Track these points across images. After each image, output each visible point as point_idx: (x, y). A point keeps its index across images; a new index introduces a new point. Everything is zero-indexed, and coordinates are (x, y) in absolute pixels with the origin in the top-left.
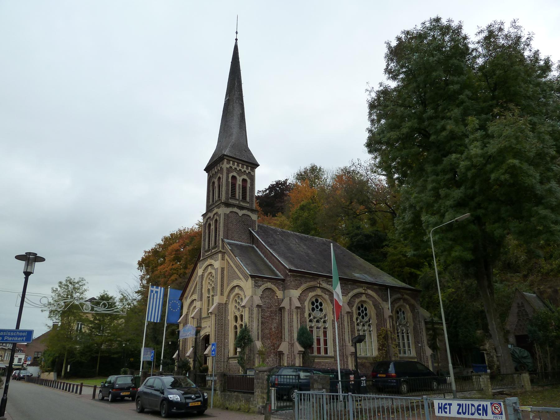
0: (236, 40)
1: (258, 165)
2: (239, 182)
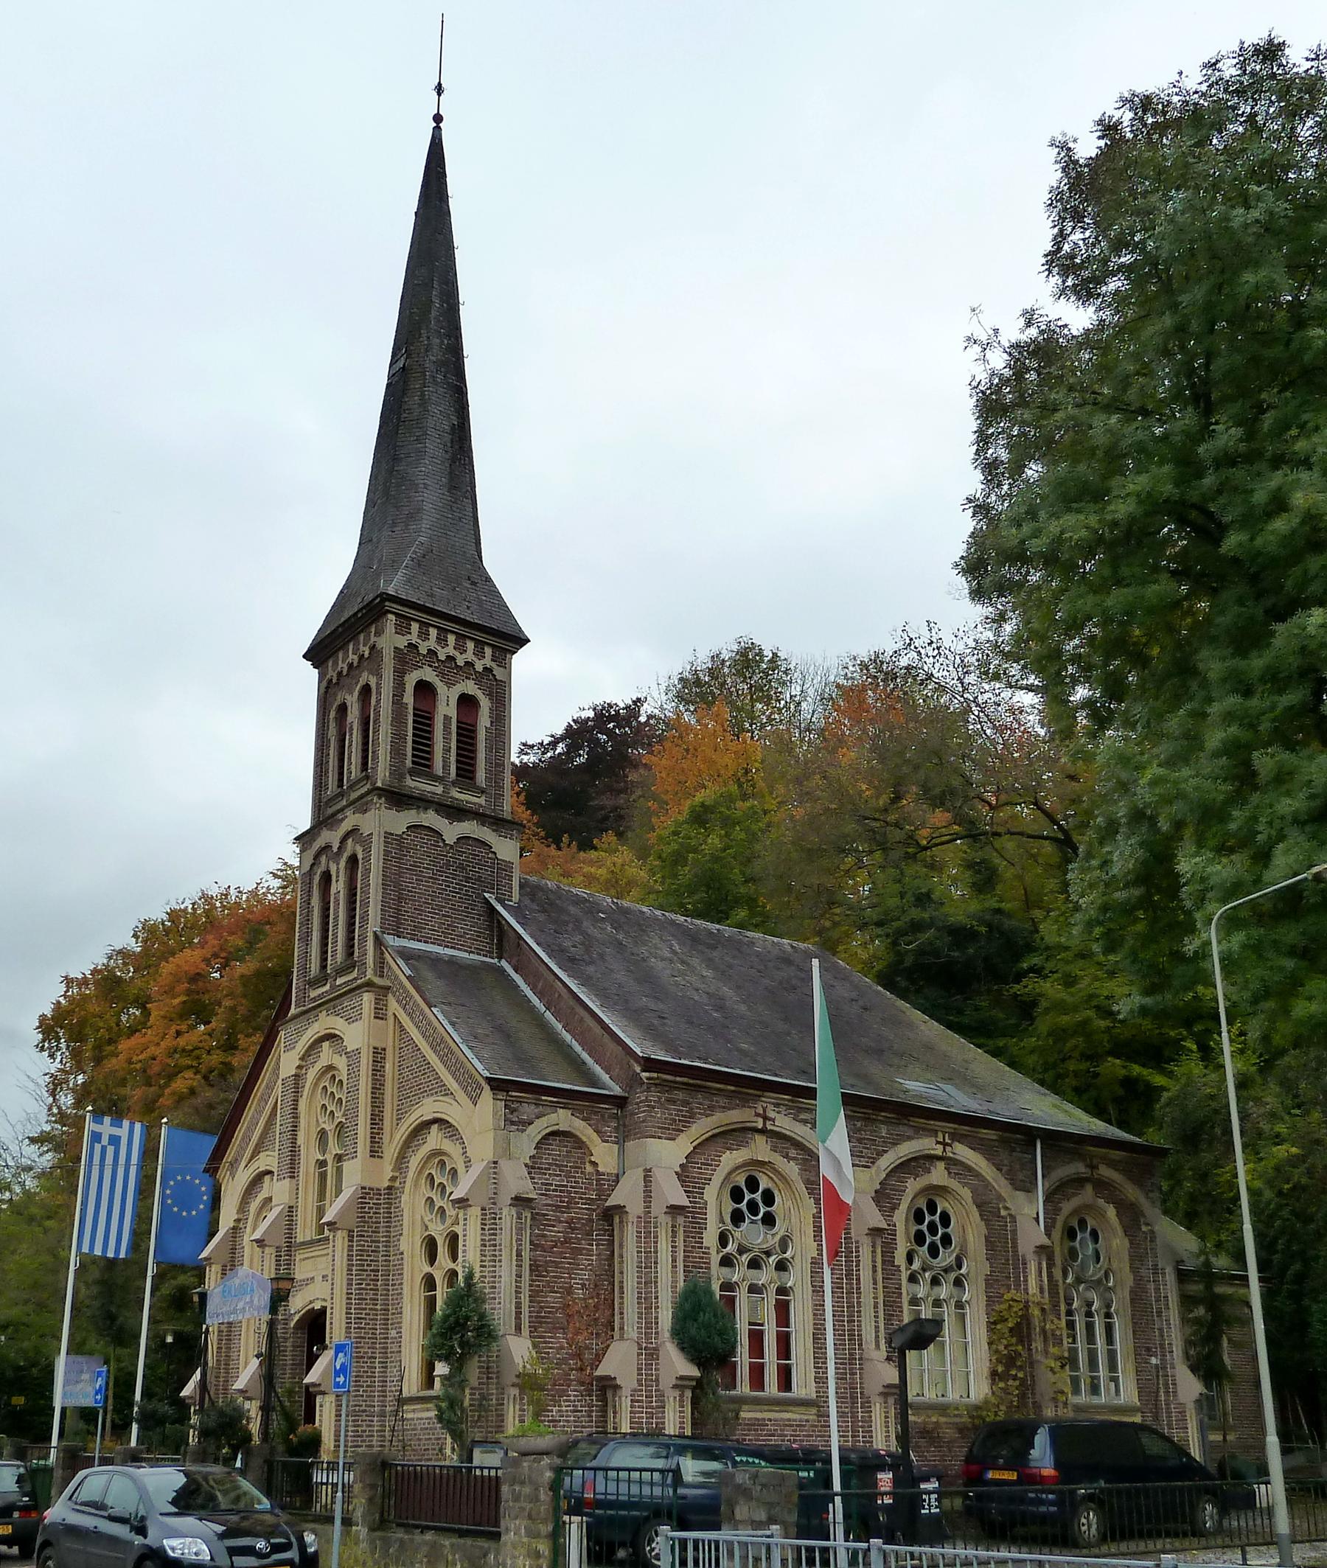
1: (523, 641)
2: (446, 707)
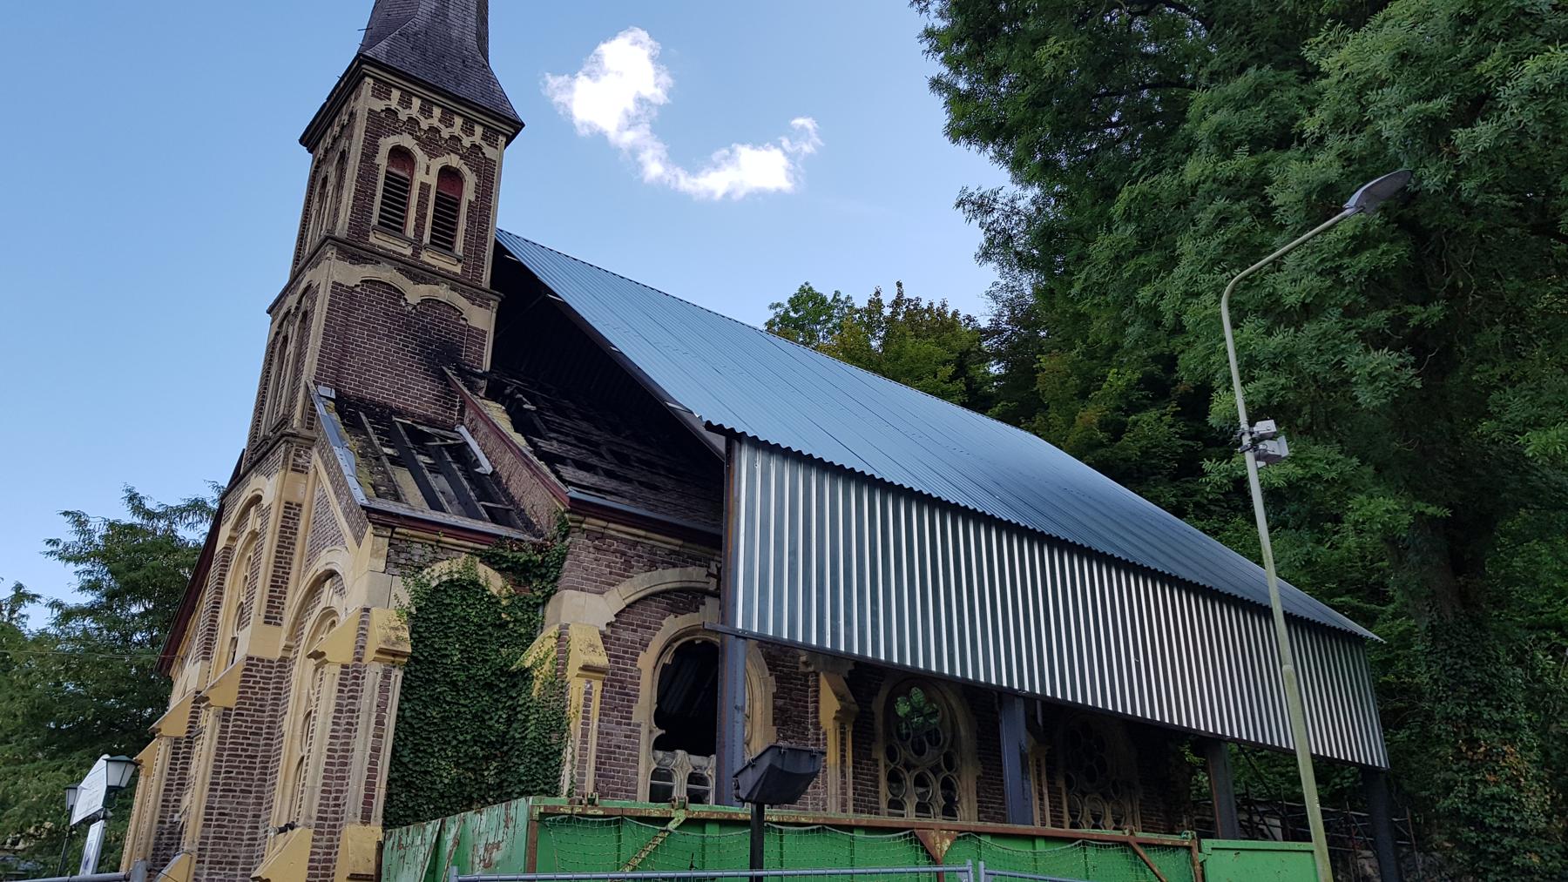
2: (426, 173)
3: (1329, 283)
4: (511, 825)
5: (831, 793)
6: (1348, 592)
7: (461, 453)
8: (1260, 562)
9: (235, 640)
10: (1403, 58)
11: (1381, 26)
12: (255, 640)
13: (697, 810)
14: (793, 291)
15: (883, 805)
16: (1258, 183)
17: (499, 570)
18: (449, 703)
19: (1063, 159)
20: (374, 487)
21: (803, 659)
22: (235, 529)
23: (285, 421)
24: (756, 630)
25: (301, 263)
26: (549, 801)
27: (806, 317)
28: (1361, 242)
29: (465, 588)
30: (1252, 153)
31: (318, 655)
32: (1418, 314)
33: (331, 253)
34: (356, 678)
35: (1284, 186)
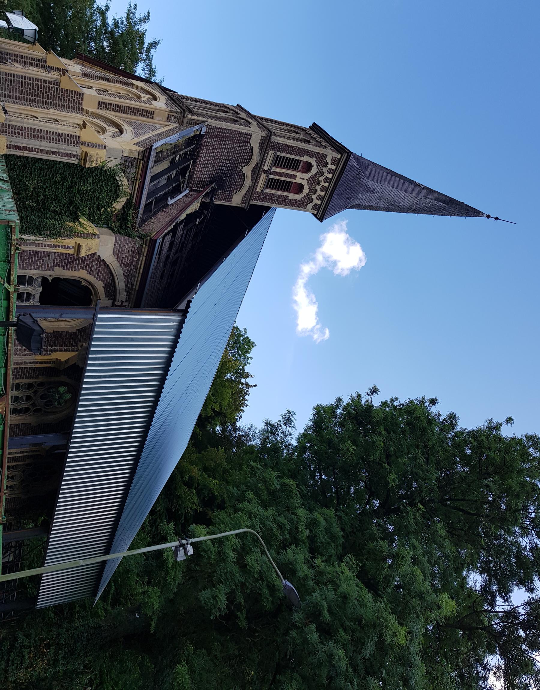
0: (488, 217)
1: (321, 222)
2: (301, 178)
3: (256, 576)
4: (6, 212)
5: (21, 357)
6: (116, 589)
7: (177, 191)
8: (129, 549)
9: (91, 88)
10: (345, 597)
11: (358, 587)
12: (91, 95)
13: (14, 297)
14: (252, 339)
15: (17, 381)
16: (296, 542)
17: (123, 208)
18: (63, 184)
19: (307, 455)
20: (161, 151)
21: (84, 344)
22: (142, 88)
23: (191, 112)
24: (97, 323)
25: (260, 120)
26: (17, 230)
27: (240, 344)
28: (272, 588)
29: (115, 192)
30: (308, 537)
31: (84, 125)
32: (242, 616)
33: (264, 134)
34: (74, 143)
35: (295, 553)
